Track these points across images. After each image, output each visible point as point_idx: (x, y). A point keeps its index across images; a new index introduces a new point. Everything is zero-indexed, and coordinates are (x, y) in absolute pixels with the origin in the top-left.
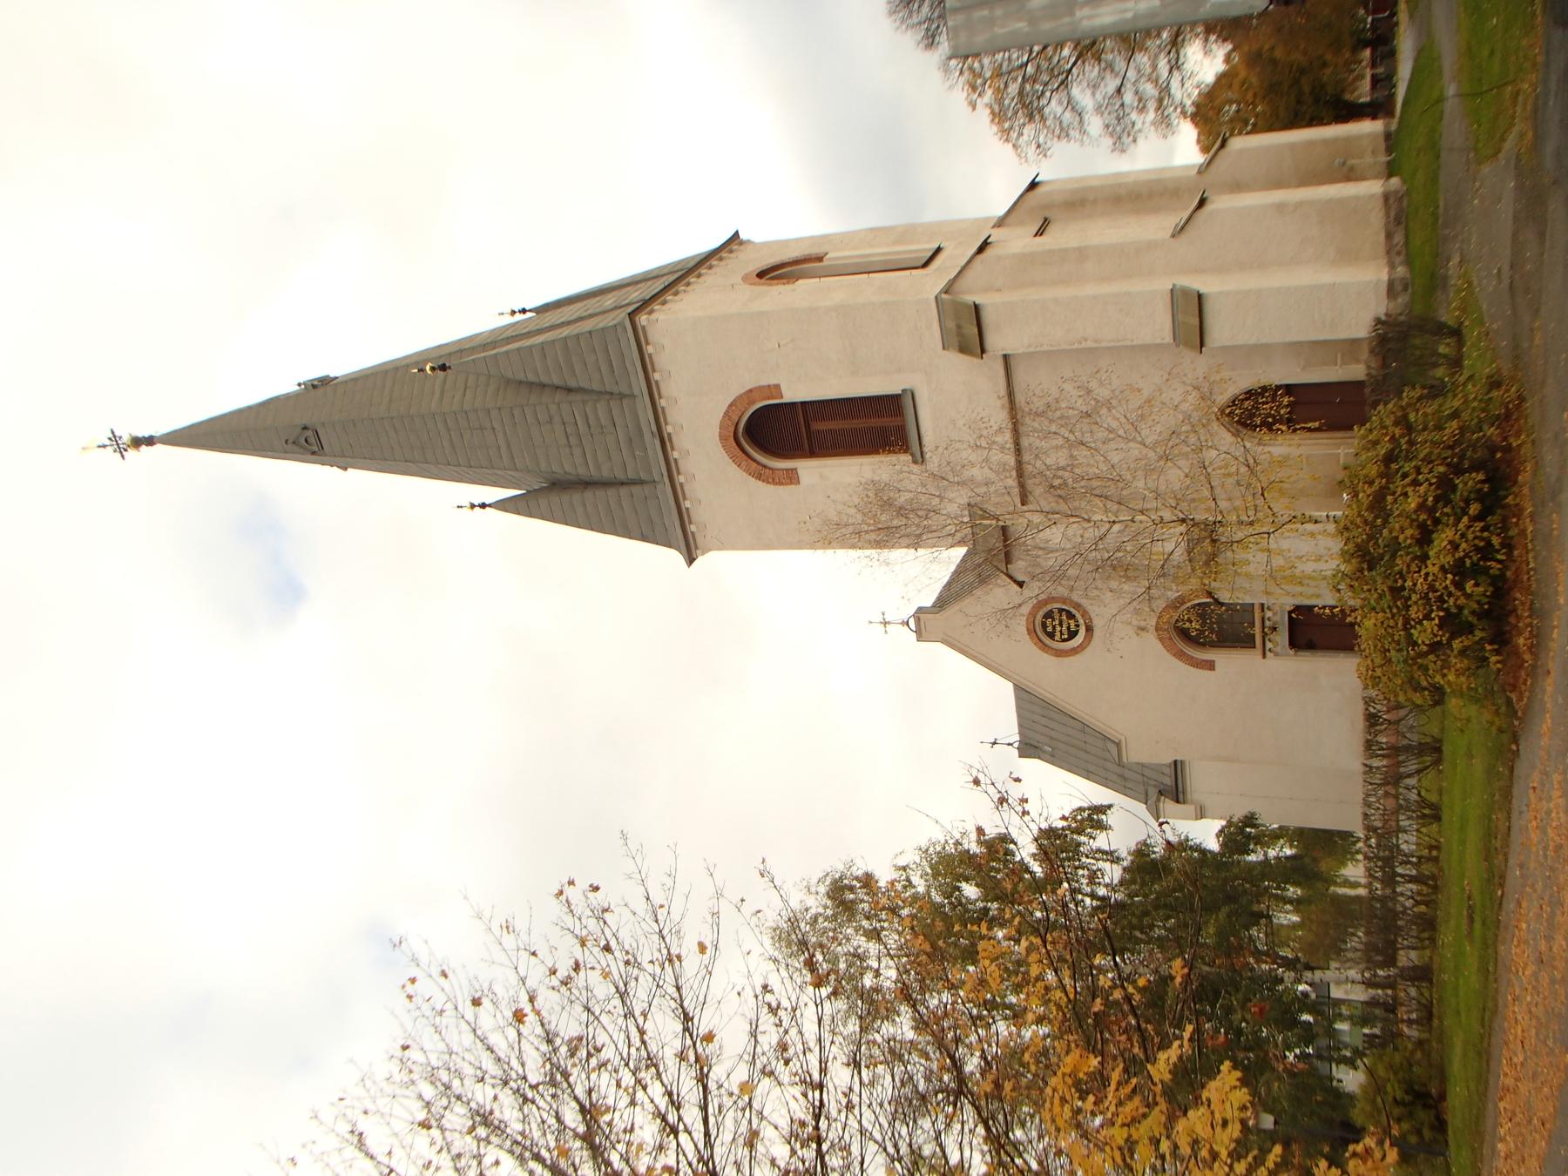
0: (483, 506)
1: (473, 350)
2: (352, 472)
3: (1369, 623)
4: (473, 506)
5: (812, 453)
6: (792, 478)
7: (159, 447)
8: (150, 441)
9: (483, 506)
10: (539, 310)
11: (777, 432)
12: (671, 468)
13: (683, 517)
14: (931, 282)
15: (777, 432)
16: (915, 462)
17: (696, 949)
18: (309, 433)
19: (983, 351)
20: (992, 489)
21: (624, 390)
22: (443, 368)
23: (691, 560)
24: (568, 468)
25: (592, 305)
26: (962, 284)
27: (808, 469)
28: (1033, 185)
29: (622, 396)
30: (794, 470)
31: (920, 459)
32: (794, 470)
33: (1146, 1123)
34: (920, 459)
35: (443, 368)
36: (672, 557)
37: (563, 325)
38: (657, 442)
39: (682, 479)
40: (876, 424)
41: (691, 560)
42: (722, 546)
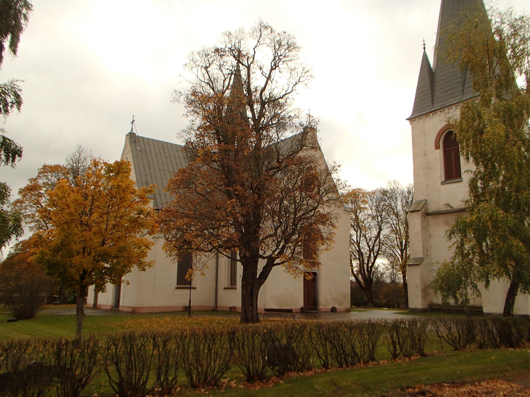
0: (424, 48)
3: (206, 139)
4: (424, 45)
5: (445, 152)
6: (437, 147)
9: (424, 48)
12: (434, 112)
13: (420, 117)
16: (442, 182)
17: (130, 282)
20: (285, 178)
21: (465, 91)
23: (407, 119)
24: (437, 77)
29: (463, 91)
30: (439, 148)
31: (442, 183)
32: (439, 148)
33: (246, 61)
34: (442, 183)
36: (409, 113)
38: (457, 101)
39: (424, 117)
41: (407, 119)
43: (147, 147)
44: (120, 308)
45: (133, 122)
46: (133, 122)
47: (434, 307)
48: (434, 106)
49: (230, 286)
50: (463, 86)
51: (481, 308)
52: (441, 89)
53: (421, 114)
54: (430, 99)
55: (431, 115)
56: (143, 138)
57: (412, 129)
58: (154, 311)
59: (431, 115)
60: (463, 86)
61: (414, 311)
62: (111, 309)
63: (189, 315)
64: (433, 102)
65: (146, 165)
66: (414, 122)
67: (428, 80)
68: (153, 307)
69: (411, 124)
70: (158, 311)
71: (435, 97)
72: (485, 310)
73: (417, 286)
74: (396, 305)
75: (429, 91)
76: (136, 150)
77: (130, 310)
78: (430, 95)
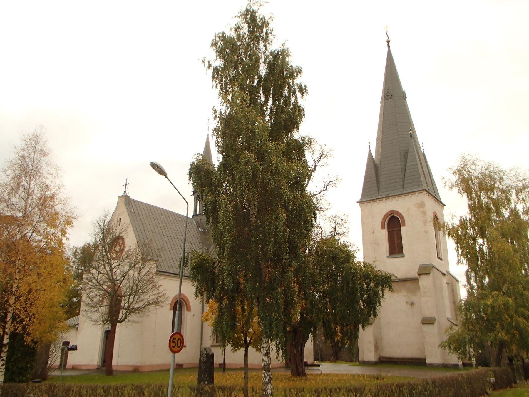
1: (416, 145)
2: (379, 105)
4: (388, 42)
5: (389, 232)
6: (383, 228)
7: (387, 48)
8: (389, 46)
9: (389, 46)
10: (423, 154)
11: (394, 223)
12: (380, 199)
13: (368, 201)
14: (436, 262)
15: (394, 223)
18: (390, 96)
19: (423, 324)
21: (405, 186)
22: (411, 136)
23: (358, 202)
25: (428, 178)
26: (434, 269)
27: (385, 232)
28: (458, 281)
29: (403, 186)
31: (388, 257)
34: (388, 257)
35: (411, 136)
36: (359, 197)
37: (421, 164)
40: (396, 247)
41: (358, 202)
42: (362, 210)
43: (139, 210)
44: (249, 367)
45: (126, 185)
46: (126, 185)
47: (382, 360)
48: (380, 194)
49: (215, 344)
50: (403, 181)
51: (425, 360)
52: (385, 181)
53: (370, 199)
54: (376, 188)
55: (378, 201)
56: (134, 200)
57: (361, 211)
58: (154, 369)
59: (378, 201)
60: (403, 181)
61: (365, 364)
62: (97, 369)
63: (224, 371)
64: (378, 191)
65: (142, 228)
66: (363, 205)
67: (373, 172)
68: (152, 366)
69: (361, 206)
70: (157, 369)
71: (380, 187)
72: (428, 361)
73: (370, 342)
74: (320, 358)
75: (375, 182)
76: (131, 212)
77: (131, 369)
78: (376, 185)
